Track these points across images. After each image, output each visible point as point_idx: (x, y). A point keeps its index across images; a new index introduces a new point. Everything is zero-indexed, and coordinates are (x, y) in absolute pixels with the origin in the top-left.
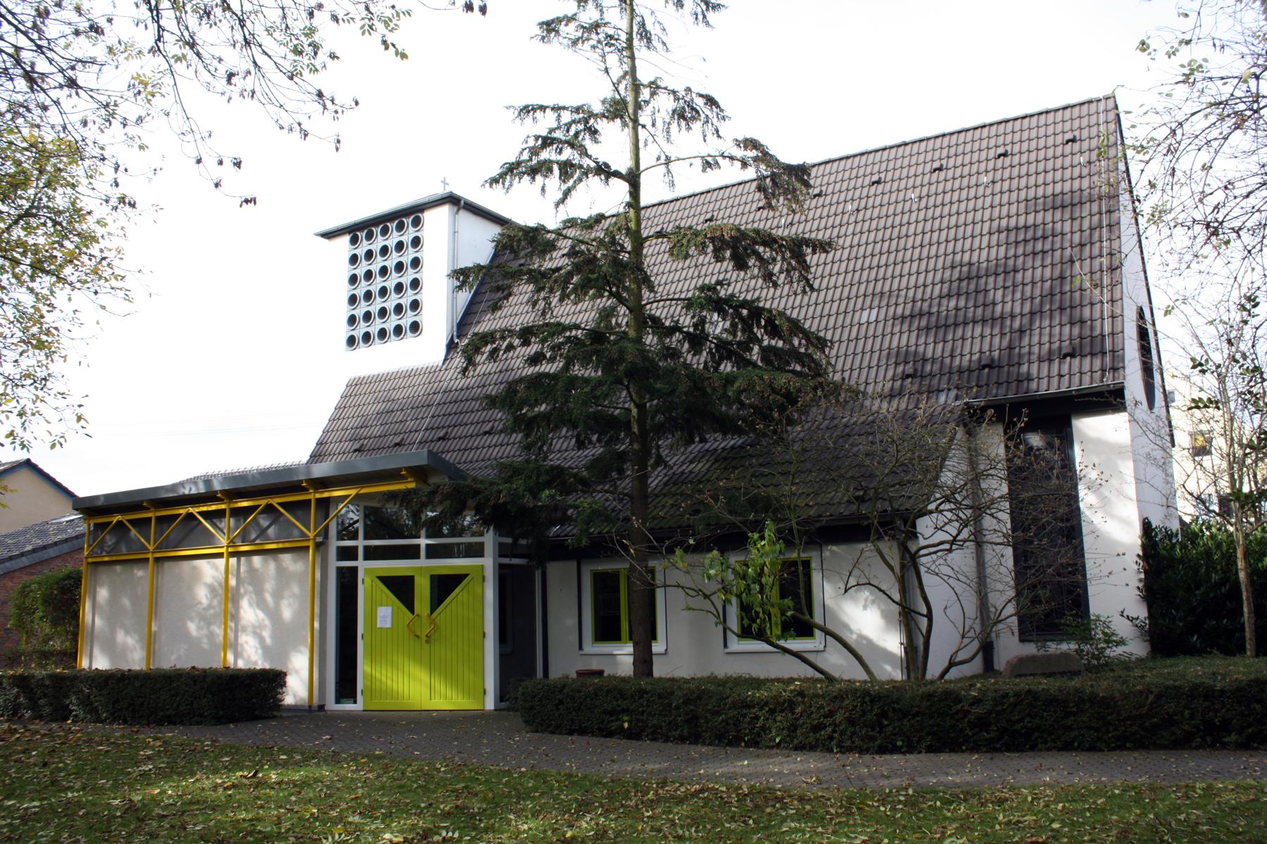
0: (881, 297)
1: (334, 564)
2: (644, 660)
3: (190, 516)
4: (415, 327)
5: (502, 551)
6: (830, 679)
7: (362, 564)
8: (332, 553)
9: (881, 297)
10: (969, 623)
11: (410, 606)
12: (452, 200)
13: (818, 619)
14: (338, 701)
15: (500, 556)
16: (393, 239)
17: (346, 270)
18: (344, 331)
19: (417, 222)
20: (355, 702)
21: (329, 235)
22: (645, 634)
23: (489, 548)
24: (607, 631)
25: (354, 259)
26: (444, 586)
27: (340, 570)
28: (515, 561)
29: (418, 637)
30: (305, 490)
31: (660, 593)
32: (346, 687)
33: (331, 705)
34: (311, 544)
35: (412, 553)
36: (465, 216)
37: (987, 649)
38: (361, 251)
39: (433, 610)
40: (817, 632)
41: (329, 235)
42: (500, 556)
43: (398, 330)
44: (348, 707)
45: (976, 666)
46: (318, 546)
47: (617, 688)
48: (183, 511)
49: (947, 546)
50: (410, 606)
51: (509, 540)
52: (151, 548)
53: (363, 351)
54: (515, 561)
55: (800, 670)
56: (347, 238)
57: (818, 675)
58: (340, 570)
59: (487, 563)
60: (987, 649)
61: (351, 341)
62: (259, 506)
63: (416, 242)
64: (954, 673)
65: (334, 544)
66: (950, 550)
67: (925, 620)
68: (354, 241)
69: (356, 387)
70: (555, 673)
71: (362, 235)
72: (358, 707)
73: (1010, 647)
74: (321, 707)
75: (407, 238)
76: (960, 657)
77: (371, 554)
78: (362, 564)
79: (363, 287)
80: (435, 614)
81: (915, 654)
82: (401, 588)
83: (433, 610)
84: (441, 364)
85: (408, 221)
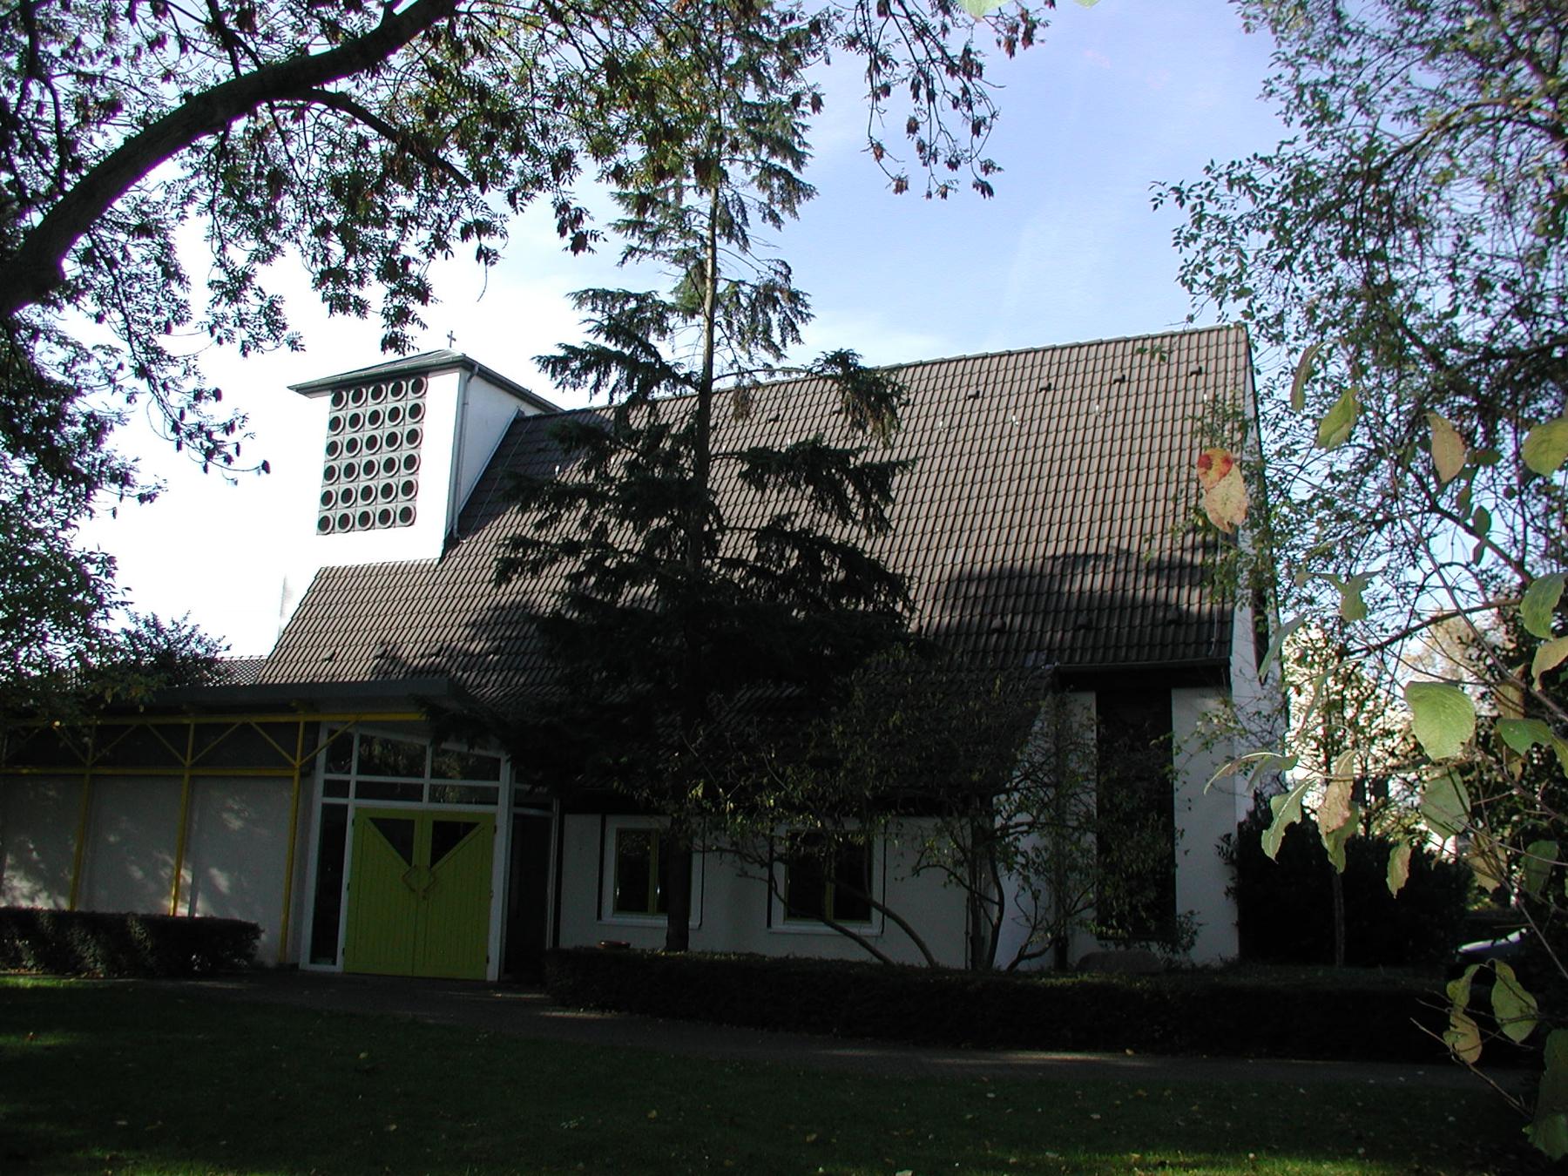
0: (1106, 561)
1: (319, 799)
2: (679, 936)
3: (246, 727)
4: (407, 516)
5: (518, 800)
6: (886, 962)
7: (352, 802)
8: (319, 788)
9: (1106, 561)
10: (1041, 912)
11: (408, 857)
12: (466, 366)
13: (877, 896)
14: (313, 960)
15: (516, 805)
16: (389, 403)
17: (322, 436)
18: (314, 510)
19: (418, 387)
20: (334, 963)
21: (307, 390)
22: (676, 906)
23: (504, 798)
24: (631, 901)
25: (334, 424)
26: (448, 835)
27: (325, 807)
28: (532, 812)
29: (413, 890)
30: (293, 711)
31: (697, 860)
32: (324, 943)
33: (304, 962)
34: (297, 774)
35: (414, 793)
36: (477, 383)
37: (1061, 945)
38: (345, 414)
39: (434, 861)
40: (876, 915)
41: (307, 390)
42: (516, 805)
43: (385, 517)
44: (323, 968)
45: (1048, 960)
46: (303, 775)
47: (647, 962)
48: (238, 720)
49: (1025, 828)
50: (408, 857)
51: (528, 787)
52: (188, 762)
53: (339, 539)
54: (532, 812)
55: (863, 955)
56: (326, 400)
57: (875, 960)
58: (325, 807)
59: (502, 813)
60: (1061, 945)
61: (324, 524)
62: (128, 727)
63: (416, 411)
64: (1023, 966)
65: (321, 776)
66: (1028, 832)
67: (996, 908)
68: (337, 401)
69: (328, 582)
70: (567, 942)
71: (347, 396)
72: (339, 967)
73: (1084, 943)
74: (295, 966)
75: (405, 404)
76: (1029, 951)
77: (364, 791)
78: (352, 802)
79: (345, 458)
80: (438, 865)
81: (980, 942)
82: (397, 833)
83: (434, 861)
84: (436, 563)
85: (407, 385)
